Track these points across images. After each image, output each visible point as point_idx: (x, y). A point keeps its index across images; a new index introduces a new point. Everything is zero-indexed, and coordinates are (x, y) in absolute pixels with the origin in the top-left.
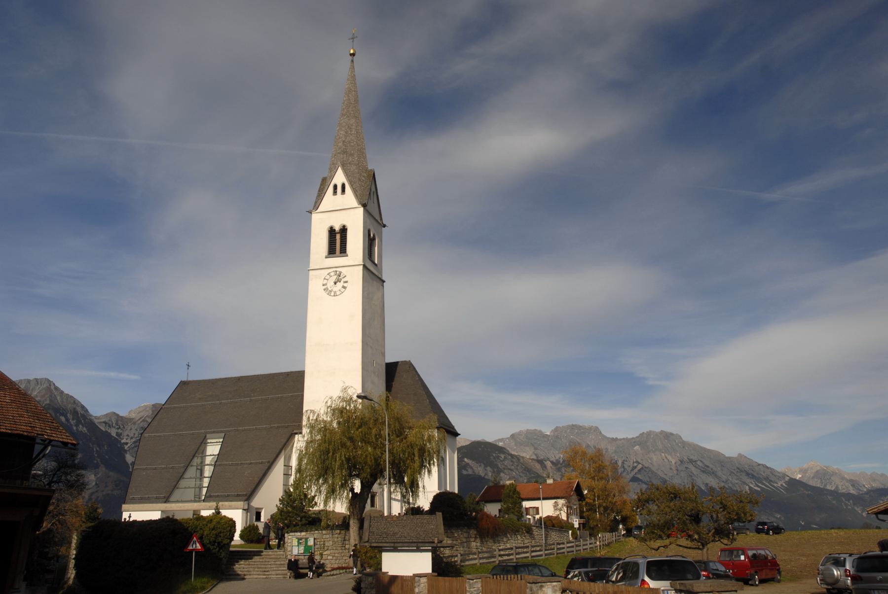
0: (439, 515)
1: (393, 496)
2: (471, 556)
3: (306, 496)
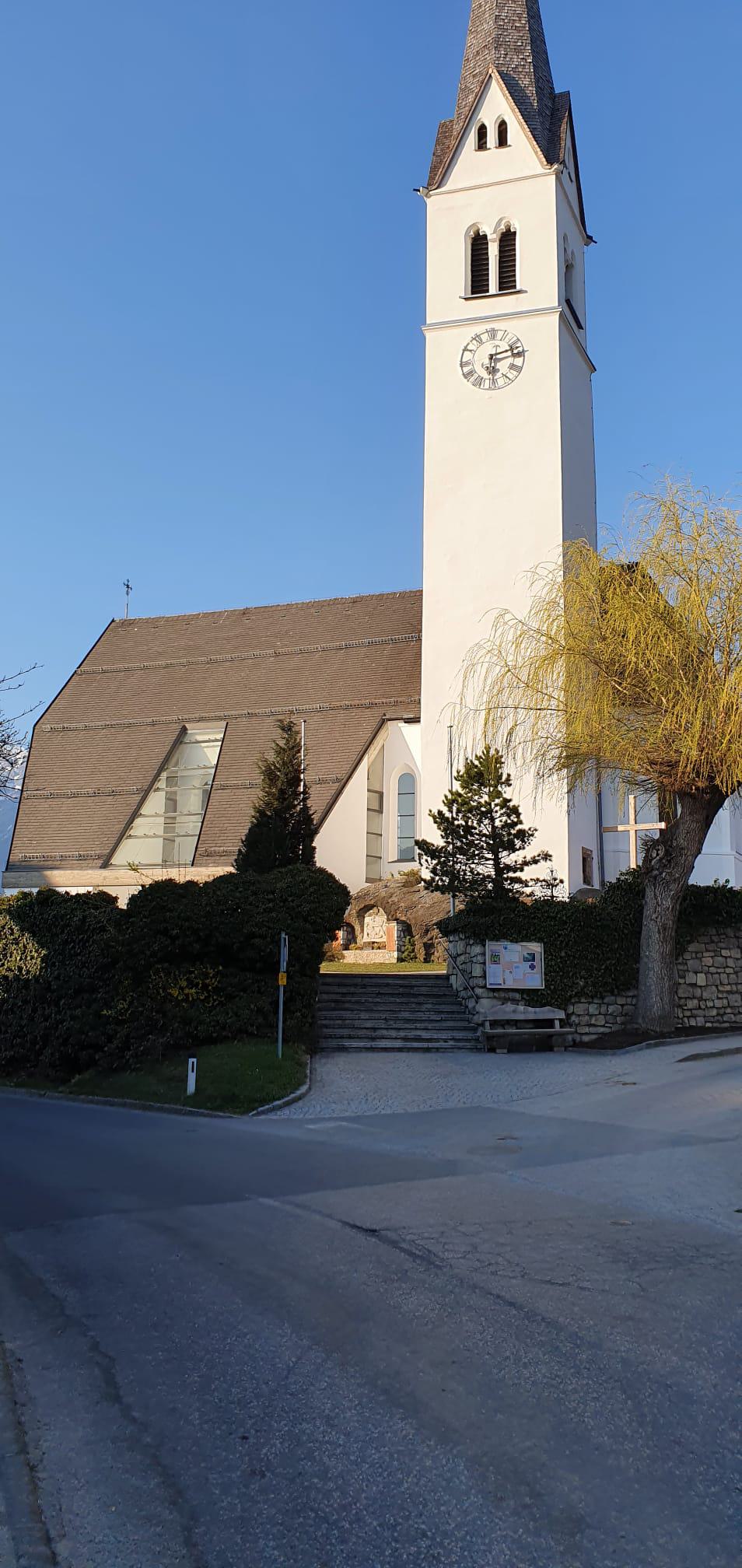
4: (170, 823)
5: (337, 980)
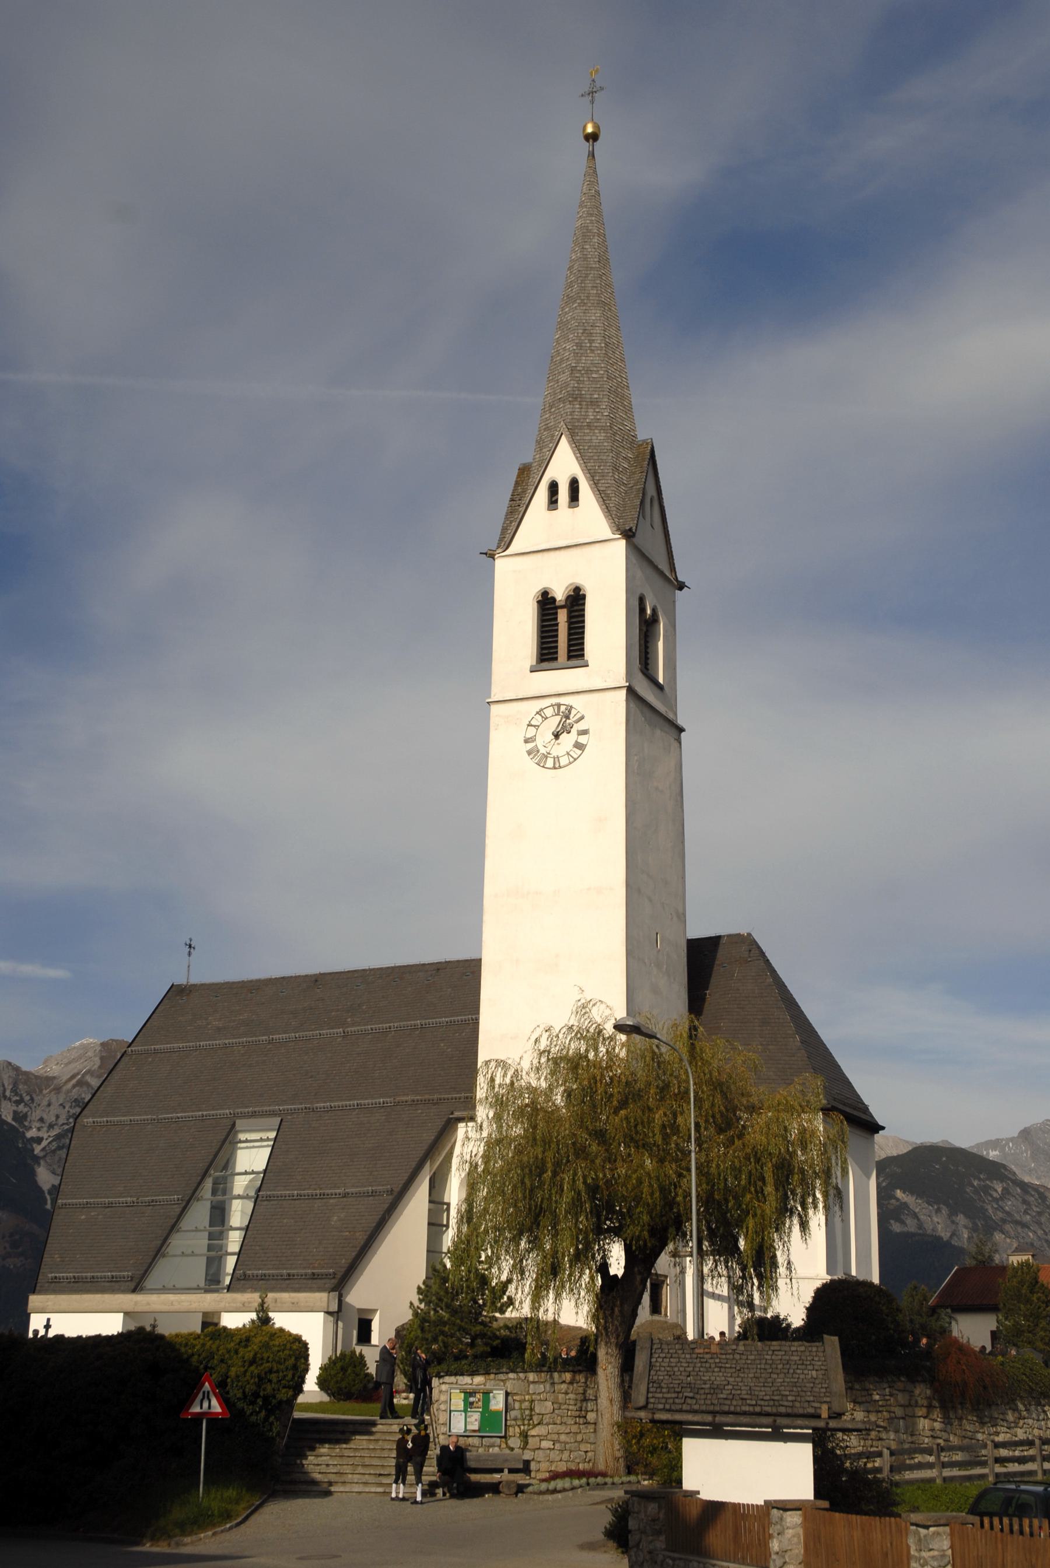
0: (832, 1342)
1: (708, 1287)
2: (919, 1458)
3: (484, 1281)
5: (508, 537)
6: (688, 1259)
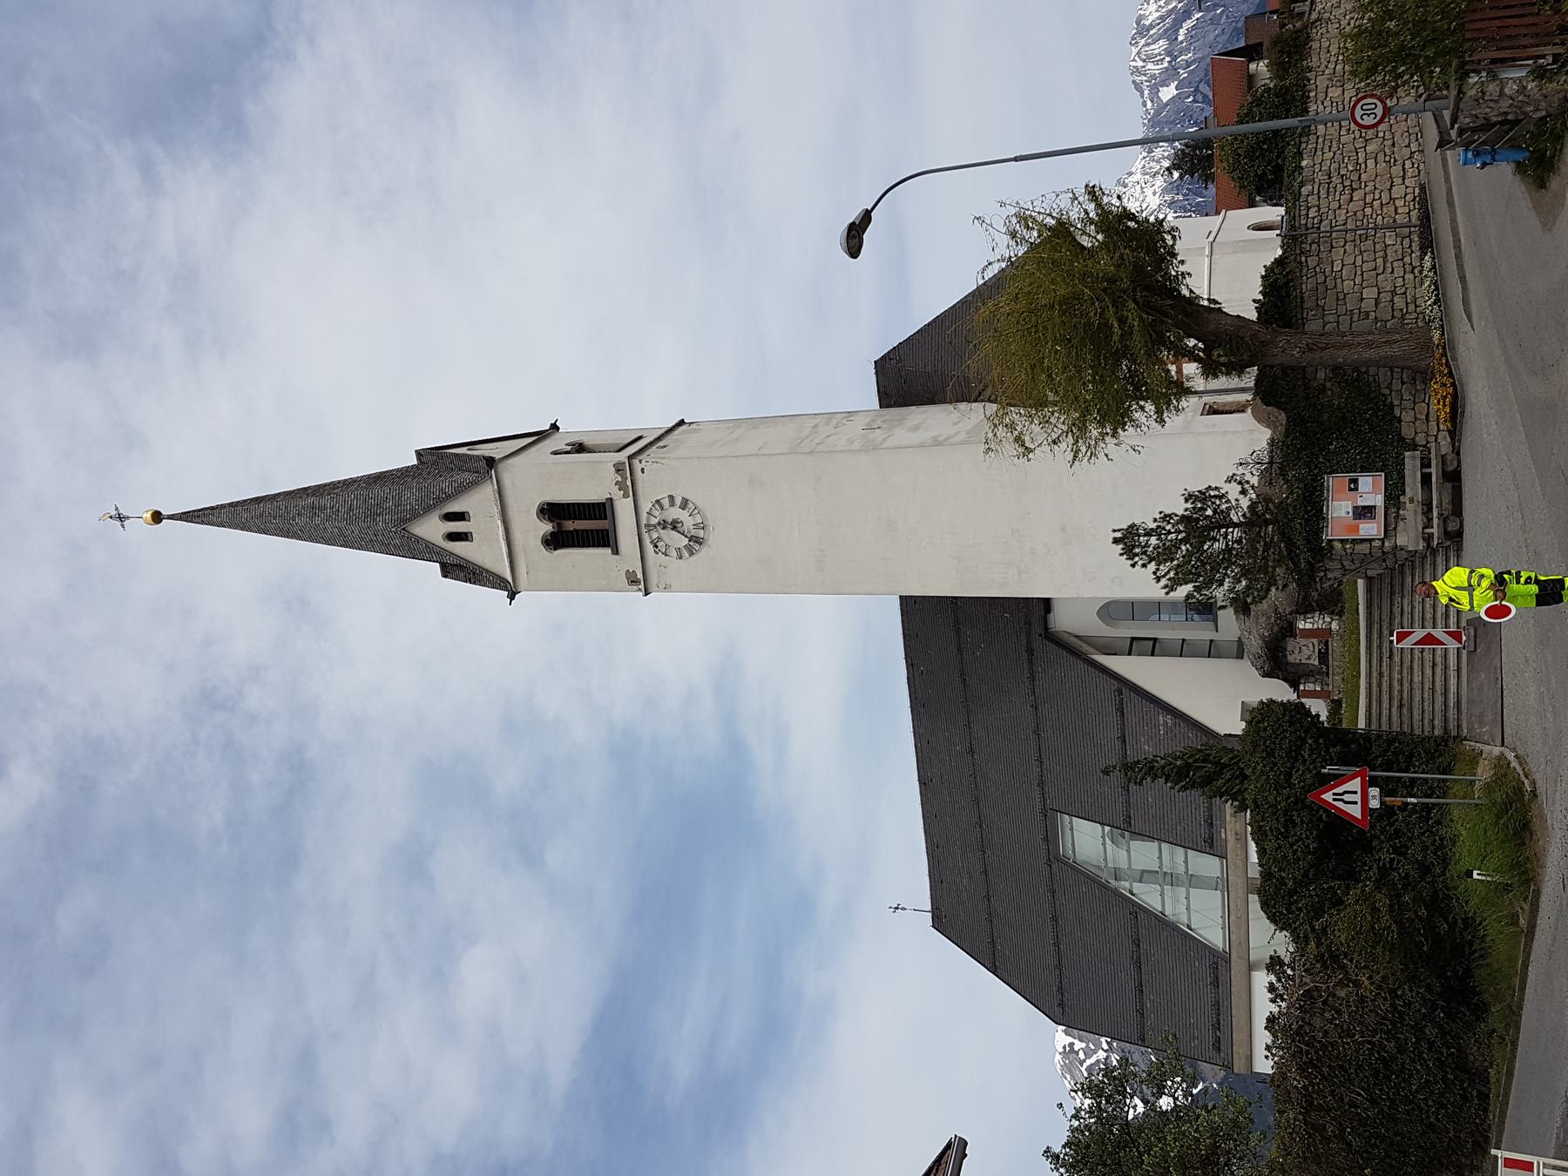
4: (1171, 879)
6: (1195, 1091)
